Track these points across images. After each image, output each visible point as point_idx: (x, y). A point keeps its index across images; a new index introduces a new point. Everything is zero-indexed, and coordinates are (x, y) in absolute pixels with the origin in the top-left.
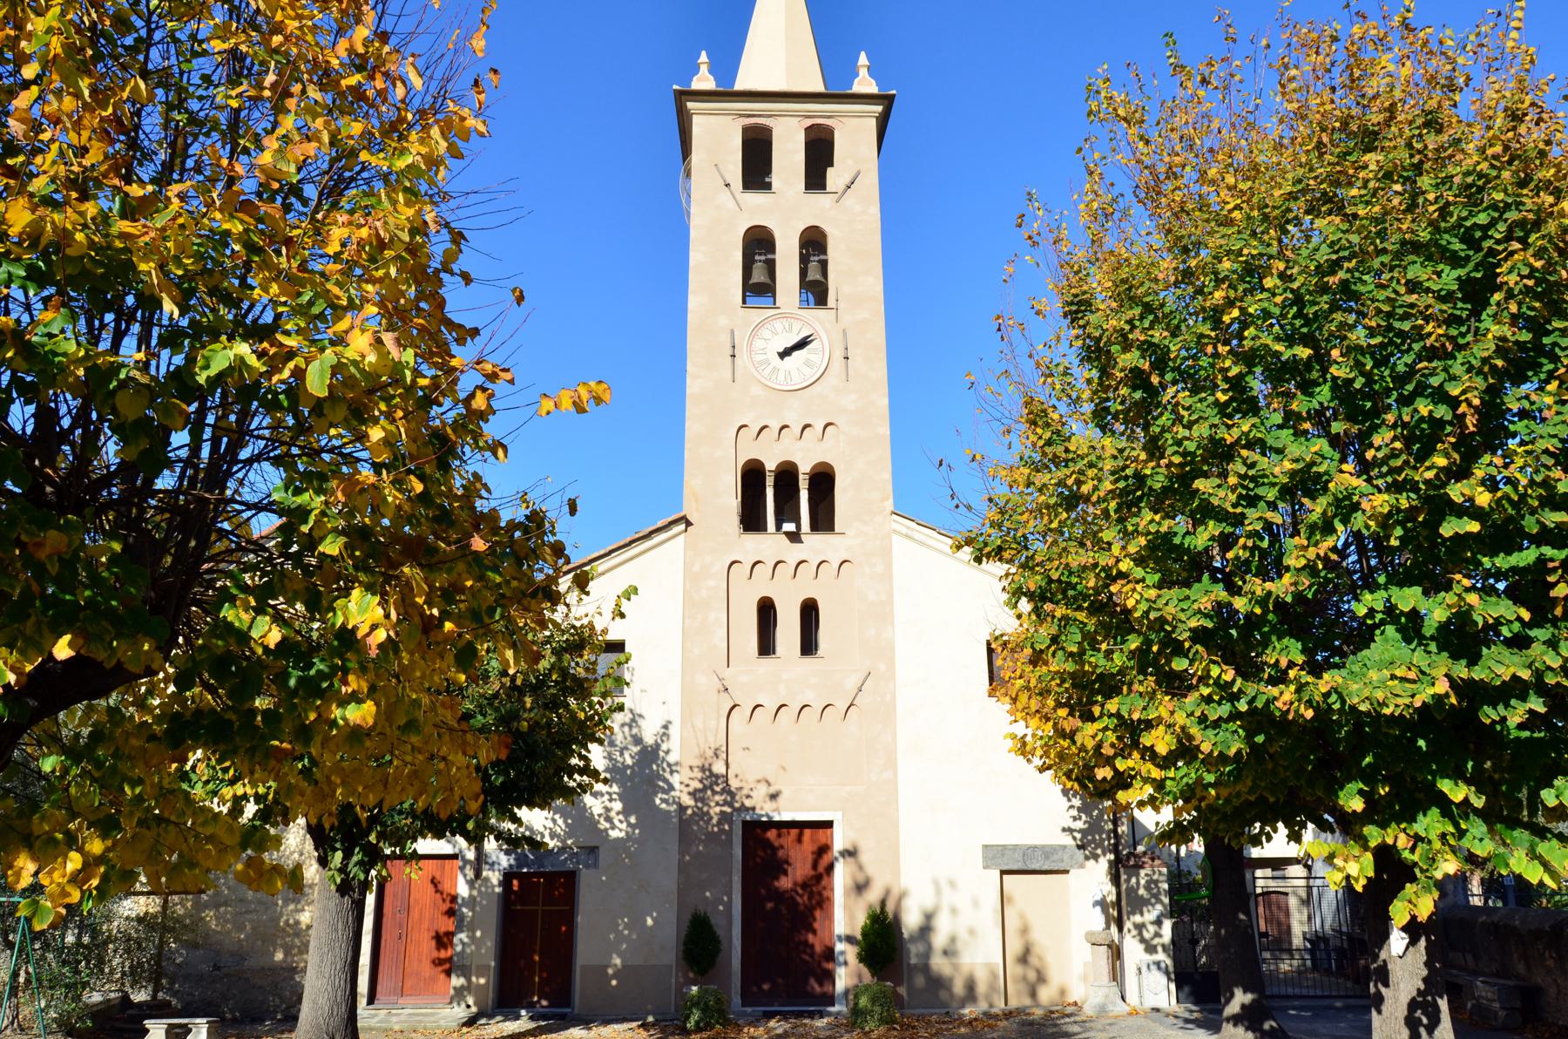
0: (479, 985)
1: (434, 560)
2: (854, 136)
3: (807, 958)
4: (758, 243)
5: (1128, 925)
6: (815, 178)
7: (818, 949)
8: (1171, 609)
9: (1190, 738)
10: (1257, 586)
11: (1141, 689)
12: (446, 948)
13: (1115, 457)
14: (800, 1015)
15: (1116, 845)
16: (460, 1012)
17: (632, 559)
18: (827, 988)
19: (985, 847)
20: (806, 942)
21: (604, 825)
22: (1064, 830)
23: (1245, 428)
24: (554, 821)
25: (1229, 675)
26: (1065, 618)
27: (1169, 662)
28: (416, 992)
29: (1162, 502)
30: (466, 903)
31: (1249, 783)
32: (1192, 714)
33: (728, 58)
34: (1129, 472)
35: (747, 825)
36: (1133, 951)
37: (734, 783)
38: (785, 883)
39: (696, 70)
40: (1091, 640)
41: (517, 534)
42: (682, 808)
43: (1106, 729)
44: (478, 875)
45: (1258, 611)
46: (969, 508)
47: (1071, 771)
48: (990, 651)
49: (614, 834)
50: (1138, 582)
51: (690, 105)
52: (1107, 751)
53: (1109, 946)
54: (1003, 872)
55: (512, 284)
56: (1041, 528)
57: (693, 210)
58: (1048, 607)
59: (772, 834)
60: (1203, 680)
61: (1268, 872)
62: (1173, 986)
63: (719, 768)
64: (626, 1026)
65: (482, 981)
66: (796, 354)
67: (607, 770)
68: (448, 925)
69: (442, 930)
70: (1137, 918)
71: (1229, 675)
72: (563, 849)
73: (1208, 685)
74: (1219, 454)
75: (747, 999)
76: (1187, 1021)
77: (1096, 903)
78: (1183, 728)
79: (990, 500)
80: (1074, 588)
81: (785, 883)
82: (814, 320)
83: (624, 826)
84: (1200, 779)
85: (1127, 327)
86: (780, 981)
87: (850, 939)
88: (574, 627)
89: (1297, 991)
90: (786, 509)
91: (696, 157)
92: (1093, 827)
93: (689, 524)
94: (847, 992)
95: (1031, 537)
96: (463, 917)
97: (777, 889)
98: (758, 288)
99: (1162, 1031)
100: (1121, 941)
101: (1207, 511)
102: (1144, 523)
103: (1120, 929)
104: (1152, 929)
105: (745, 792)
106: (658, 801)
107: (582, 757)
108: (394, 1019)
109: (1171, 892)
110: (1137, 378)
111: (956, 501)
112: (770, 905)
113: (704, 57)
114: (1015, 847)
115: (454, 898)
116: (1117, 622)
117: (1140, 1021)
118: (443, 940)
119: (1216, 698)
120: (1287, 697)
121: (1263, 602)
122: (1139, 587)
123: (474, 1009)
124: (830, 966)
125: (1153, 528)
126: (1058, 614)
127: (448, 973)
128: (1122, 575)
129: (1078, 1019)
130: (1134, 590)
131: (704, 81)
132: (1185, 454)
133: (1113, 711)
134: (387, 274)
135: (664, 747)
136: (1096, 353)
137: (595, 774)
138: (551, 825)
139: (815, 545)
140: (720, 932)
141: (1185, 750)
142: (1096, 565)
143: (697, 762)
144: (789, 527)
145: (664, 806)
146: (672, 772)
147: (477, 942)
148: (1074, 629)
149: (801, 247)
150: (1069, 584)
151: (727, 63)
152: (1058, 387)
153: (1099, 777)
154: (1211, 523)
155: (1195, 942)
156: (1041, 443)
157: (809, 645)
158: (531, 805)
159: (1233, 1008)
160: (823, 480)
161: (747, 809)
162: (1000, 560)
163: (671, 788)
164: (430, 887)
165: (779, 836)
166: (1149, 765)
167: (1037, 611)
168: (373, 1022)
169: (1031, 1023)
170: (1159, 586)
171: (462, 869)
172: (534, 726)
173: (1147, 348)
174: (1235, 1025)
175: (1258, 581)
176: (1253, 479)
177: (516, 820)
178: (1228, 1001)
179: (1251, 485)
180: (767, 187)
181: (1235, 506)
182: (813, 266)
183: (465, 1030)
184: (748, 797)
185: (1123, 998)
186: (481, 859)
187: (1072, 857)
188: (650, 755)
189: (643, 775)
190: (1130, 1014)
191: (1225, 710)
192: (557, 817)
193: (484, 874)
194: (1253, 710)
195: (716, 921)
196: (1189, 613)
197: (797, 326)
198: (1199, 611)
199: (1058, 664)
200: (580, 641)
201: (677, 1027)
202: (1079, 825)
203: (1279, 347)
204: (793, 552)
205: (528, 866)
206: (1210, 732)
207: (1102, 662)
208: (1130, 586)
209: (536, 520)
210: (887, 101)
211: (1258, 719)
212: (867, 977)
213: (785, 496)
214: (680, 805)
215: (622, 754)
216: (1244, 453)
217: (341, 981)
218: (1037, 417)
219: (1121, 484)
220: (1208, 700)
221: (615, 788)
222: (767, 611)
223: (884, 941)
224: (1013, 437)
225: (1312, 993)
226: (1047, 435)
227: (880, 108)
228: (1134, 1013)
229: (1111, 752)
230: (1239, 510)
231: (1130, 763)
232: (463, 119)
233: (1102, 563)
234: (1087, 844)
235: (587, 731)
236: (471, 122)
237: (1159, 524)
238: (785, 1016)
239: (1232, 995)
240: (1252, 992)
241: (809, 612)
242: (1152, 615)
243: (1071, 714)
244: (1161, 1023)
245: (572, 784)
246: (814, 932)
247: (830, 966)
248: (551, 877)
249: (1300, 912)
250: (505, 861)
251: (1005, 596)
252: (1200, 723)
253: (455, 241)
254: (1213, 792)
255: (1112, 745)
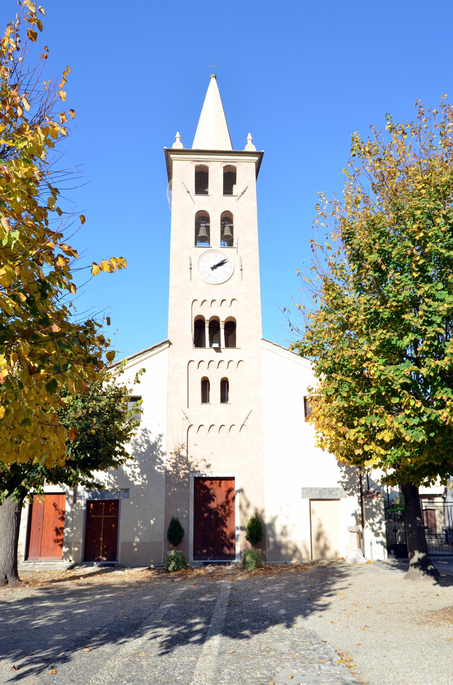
0: (75, 551)
1: (38, 341)
2: (245, 170)
3: (223, 538)
4: (202, 218)
5: (366, 524)
6: (228, 189)
7: (228, 533)
8: (391, 374)
9: (401, 434)
10: (433, 363)
11: (377, 411)
12: (60, 534)
13: (366, 304)
14: (219, 564)
15: (361, 489)
16: (66, 563)
17: (145, 359)
18: (232, 552)
19: (303, 488)
20: (223, 532)
21: (132, 479)
22: (338, 482)
23: (426, 289)
24: (109, 477)
25: (419, 404)
26: (341, 380)
27: (390, 400)
28: (47, 554)
29: (387, 324)
30: (69, 514)
31: (426, 456)
32: (401, 423)
33: (189, 134)
34: (372, 310)
35: (196, 479)
36: (368, 534)
37: (190, 460)
38: (213, 505)
39: (175, 140)
40: (353, 391)
41: (81, 332)
42: (167, 472)
43: (359, 432)
44: (75, 502)
45: (432, 374)
46: (298, 330)
47: (343, 452)
48: (305, 400)
49: (136, 483)
50: (375, 362)
51: (172, 156)
52: (360, 441)
53: (358, 533)
54: (311, 500)
55: (80, 214)
56: (331, 340)
57: (173, 203)
58: (333, 375)
59: (207, 483)
60: (407, 407)
61: (427, 500)
62: (386, 551)
63: (183, 453)
64: (141, 569)
65: (76, 549)
66: (219, 268)
67: (133, 454)
68: (61, 524)
69: (59, 527)
70: (371, 521)
71: (419, 404)
72: (113, 490)
73: (409, 409)
74: (414, 303)
75: (196, 556)
76: (393, 566)
77: (353, 515)
78: (397, 429)
79: (307, 327)
80: (346, 367)
81: (213, 505)
82: (227, 253)
83: (141, 479)
84: (403, 454)
85: (372, 242)
86: (211, 548)
87: (242, 528)
88: (117, 388)
89: (441, 553)
90: (214, 337)
91: (174, 179)
92: (352, 480)
93: (170, 344)
94: (241, 553)
95: (325, 345)
96: (68, 520)
97: (209, 507)
98: (202, 238)
99: (382, 570)
100: (363, 531)
101: (408, 329)
102: (378, 334)
103: (363, 526)
104: (378, 525)
105: (195, 463)
106: (156, 468)
107: (121, 447)
108: (36, 567)
109: (385, 510)
110: (376, 267)
111: (291, 328)
112: (206, 515)
113: (178, 135)
114: (316, 489)
115: (64, 512)
116: (365, 382)
117: (372, 566)
118: (59, 531)
119: (412, 415)
120: (445, 415)
121: (434, 370)
122: (376, 365)
123: (73, 562)
124: (233, 541)
125: (382, 337)
126: (338, 378)
127: (61, 546)
128: (368, 359)
129: (344, 565)
130: (374, 366)
131: (178, 145)
132: (398, 301)
133: (363, 423)
134: (15, 200)
135: (159, 444)
136: (357, 257)
137: (127, 455)
138: (108, 479)
139: (227, 353)
140: (184, 527)
141: (397, 441)
142: (356, 355)
143: (173, 451)
144: (216, 345)
145: (159, 470)
146: (162, 455)
147: (75, 532)
148: (345, 385)
149: (221, 221)
150: (343, 365)
151: (189, 136)
152: (338, 274)
153: (356, 454)
154: (410, 334)
155: (396, 531)
156: (331, 298)
157: (224, 399)
158: (97, 468)
159: (415, 560)
160: (231, 325)
161: (196, 472)
162: (312, 354)
163: (162, 462)
164: (53, 508)
165: (211, 484)
166: (379, 448)
167: (329, 378)
168: (27, 568)
169: (323, 567)
170: (385, 364)
171: (67, 499)
172: (98, 431)
173: (381, 252)
174: (415, 567)
175: (433, 360)
176: (430, 312)
177: (91, 476)
178: (412, 557)
179: (430, 316)
180: (207, 193)
181: (422, 325)
182: (227, 229)
183: (68, 571)
184: (197, 466)
185: (364, 556)
186: (76, 495)
187: (341, 493)
188: (153, 447)
189: (149, 456)
190: (367, 563)
191: (416, 421)
192: (111, 475)
193: (78, 501)
194: (429, 422)
195: (183, 522)
196: (399, 377)
197: (219, 255)
198: (404, 375)
199: (337, 403)
200: (119, 395)
201: (165, 570)
202: (346, 480)
203: (443, 251)
204: (217, 357)
205: (98, 498)
206: (410, 431)
207: (359, 401)
208: (372, 364)
209: (90, 325)
210: (260, 155)
211: (431, 426)
212: (249, 544)
213: (212, 331)
214: (166, 470)
215: (140, 448)
216: (427, 300)
217: (10, 550)
218: (329, 287)
219: (369, 316)
220: (409, 416)
221: (137, 463)
222: (205, 383)
223: (258, 530)
224: (318, 298)
225: (448, 553)
226: (334, 295)
227: (257, 158)
228: (369, 563)
229: (362, 442)
230: (424, 328)
231: (371, 447)
232: (54, 127)
233: (359, 354)
234: (347, 487)
235: (123, 436)
236: (58, 128)
237: (385, 334)
238: (213, 564)
239: (414, 554)
240: (423, 552)
241: (225, 383)
242: (382, 378)
243: (343, 425)
244: (381, 567)
245: (117, 460)
246: (227, 527)
247: (233, 541)
248: (108, 502)
249: (440, 517)
250: (87, 495)
251: (314, 372)
252: (405, 427)
253: (53, 193)
254: (409, 460)
255: (363, 439)
